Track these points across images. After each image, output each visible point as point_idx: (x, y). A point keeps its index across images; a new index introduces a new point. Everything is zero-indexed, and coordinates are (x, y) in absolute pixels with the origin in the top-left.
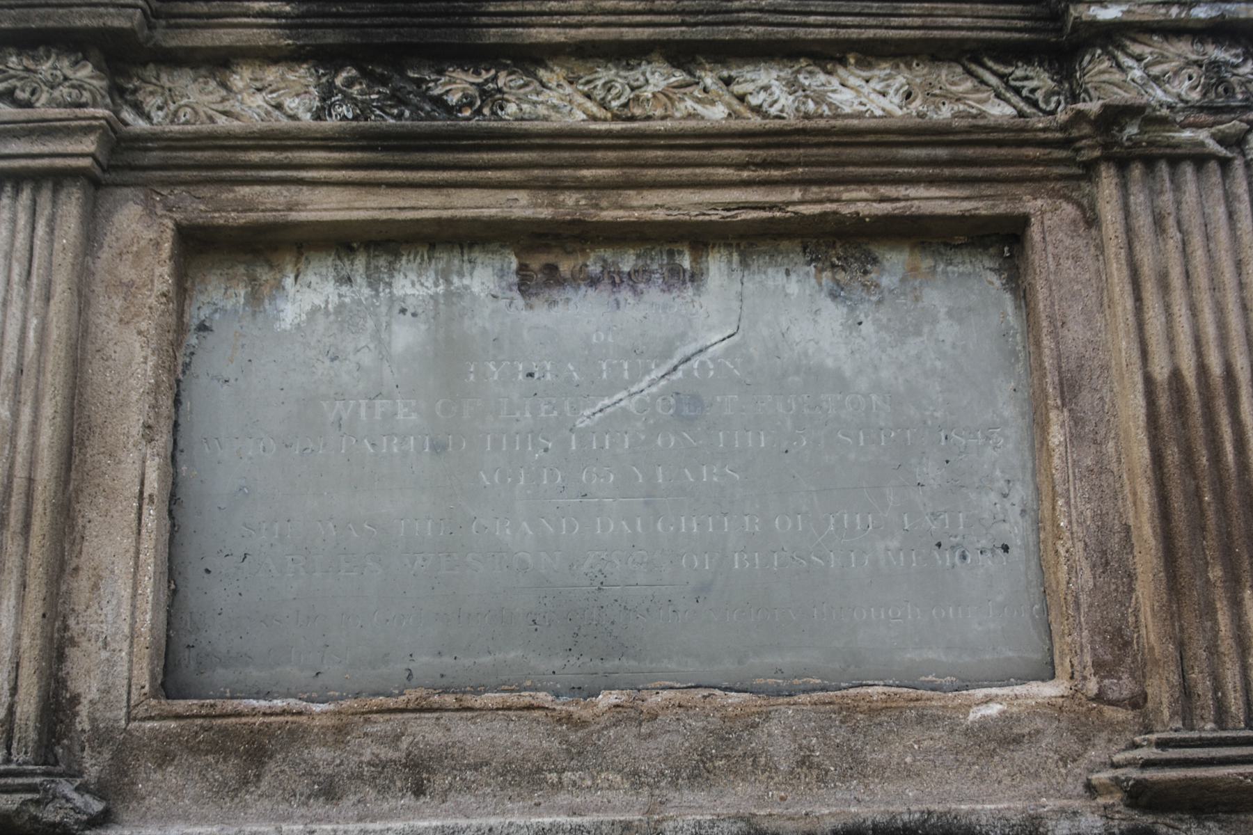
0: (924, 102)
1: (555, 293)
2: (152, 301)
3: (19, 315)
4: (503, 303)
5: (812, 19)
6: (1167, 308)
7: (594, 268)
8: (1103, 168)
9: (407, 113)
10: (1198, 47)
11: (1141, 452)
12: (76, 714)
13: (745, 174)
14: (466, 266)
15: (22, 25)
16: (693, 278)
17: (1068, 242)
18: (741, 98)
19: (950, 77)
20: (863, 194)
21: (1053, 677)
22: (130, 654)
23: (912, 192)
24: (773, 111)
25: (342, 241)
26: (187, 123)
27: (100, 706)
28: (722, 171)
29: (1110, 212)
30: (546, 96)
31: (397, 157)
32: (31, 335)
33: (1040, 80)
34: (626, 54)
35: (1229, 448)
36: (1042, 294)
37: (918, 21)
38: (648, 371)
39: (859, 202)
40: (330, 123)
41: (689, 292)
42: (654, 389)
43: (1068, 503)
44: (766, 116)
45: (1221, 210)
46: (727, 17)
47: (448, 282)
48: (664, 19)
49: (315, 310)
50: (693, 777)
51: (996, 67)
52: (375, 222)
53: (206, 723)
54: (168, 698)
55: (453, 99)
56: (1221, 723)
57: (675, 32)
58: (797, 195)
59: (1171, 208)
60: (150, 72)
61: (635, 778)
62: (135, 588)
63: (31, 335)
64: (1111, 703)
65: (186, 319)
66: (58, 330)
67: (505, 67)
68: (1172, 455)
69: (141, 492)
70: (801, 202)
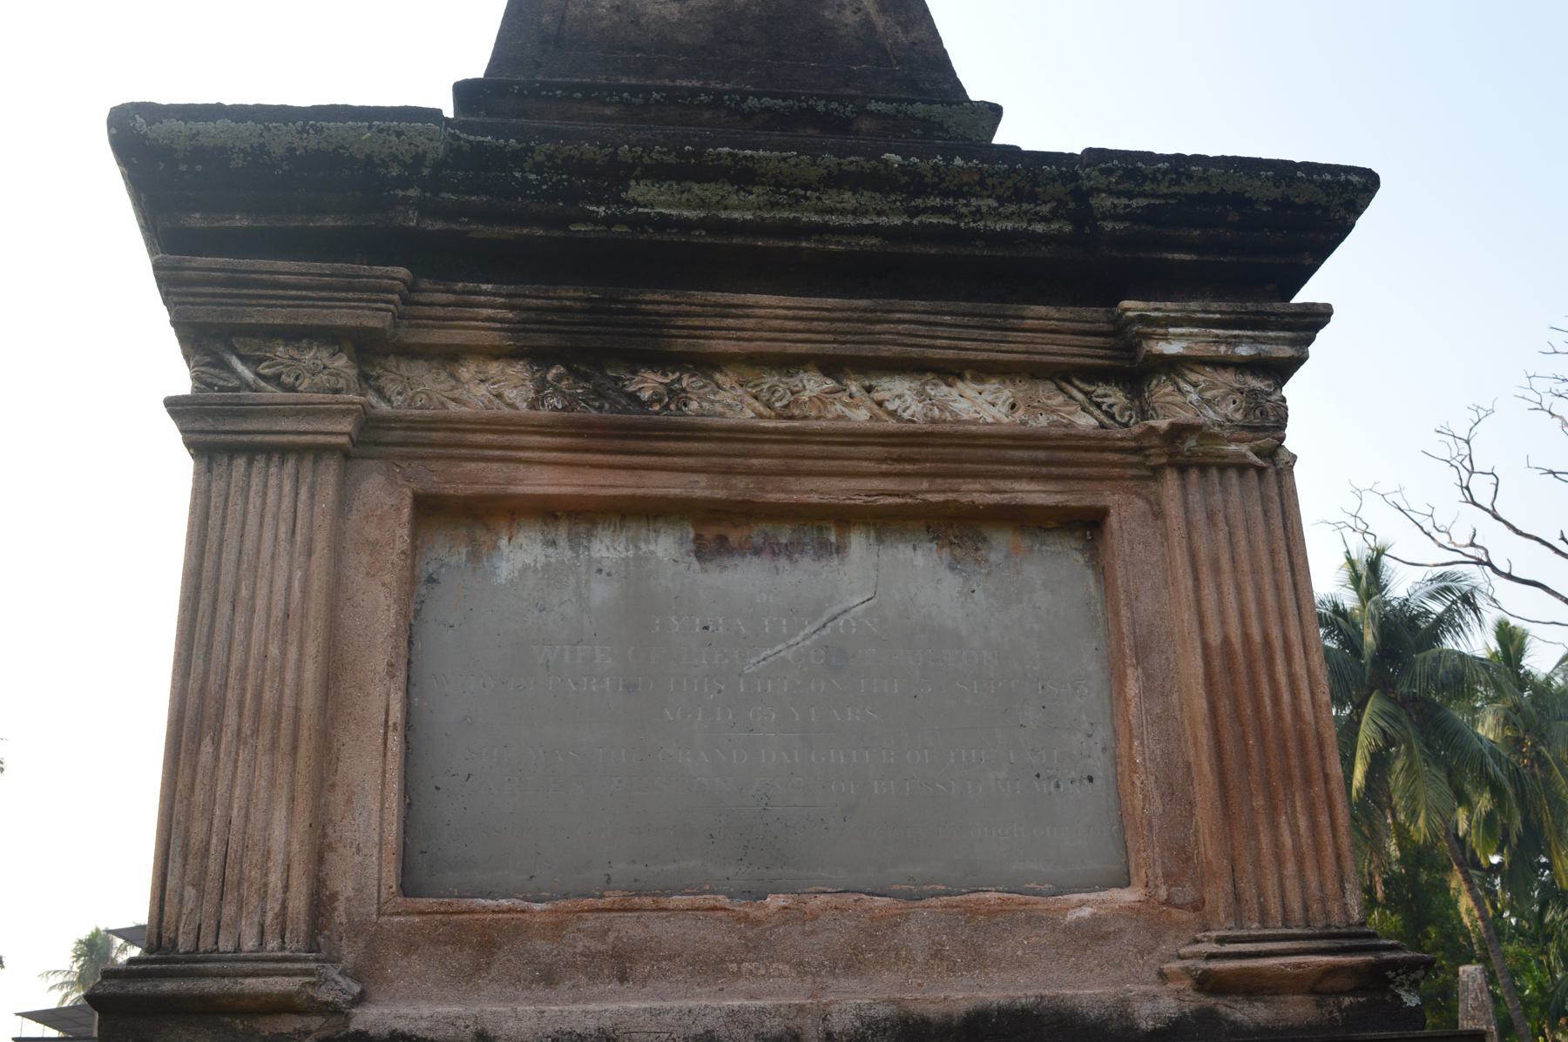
0: (1026, 412)
1: (726, 561)
2: (394, 558)
3: (285, 566)
4: (682, 566)
5: (939, 342)
6: (1219, 587)
7: (758, 540)
8: (1168, 471)
9: (607, 406)
10: (1240, 377)
11: (1201, 704)
12: (335, 909)
13: (884, 467)
14: (652, 535)
15: (293, 322)
16: (838, 552)
17: (1139, 530)
18: (880, 404)
19: (1048, 394)
20: (978, 486)
21: (1128, 884)
22: (380, 858)
23: (1017, 486)
24: (906, 415)
25: (547, 511)
26: (421, 408)
27: (355, 903)
28: (865, 464)
29: (1173, 509)
30: (722, 396)
31: (600, 443)
32: (296, 584)
33: (1115, 397)
34: (789, 364)
35: (1267, 701)
36: (1120, 572)
37: (1022, 347)
38: (803, 627)
39: (977, 493)
40: (544, 413)
41: (835, 561)
42: (808, 642)
43: (1142, 743)
44: (900, 419)
45: (1259, 509)
46: (871, 337)
47: (637, 548)
48: (820, 337)
49: (525, 569)
50: (847, 967)
51: (1082, 386)
52: (580, 496)
53: (445, 918)
54: (405, 895)
55: (645, 395)
56: (1238, 918)
57: (829, 349)
58: (925, 485)
59: (1220, 506)
60: (391, 362)
61: (800, 967)
62: (382, 804)
63: (296, 584)
64: (1177, 907)
65: (417, 571)
66: (318, 583)
67: (688, 370)
68: (1225, 706)
69: (386, 721)
70: (929, 492)
